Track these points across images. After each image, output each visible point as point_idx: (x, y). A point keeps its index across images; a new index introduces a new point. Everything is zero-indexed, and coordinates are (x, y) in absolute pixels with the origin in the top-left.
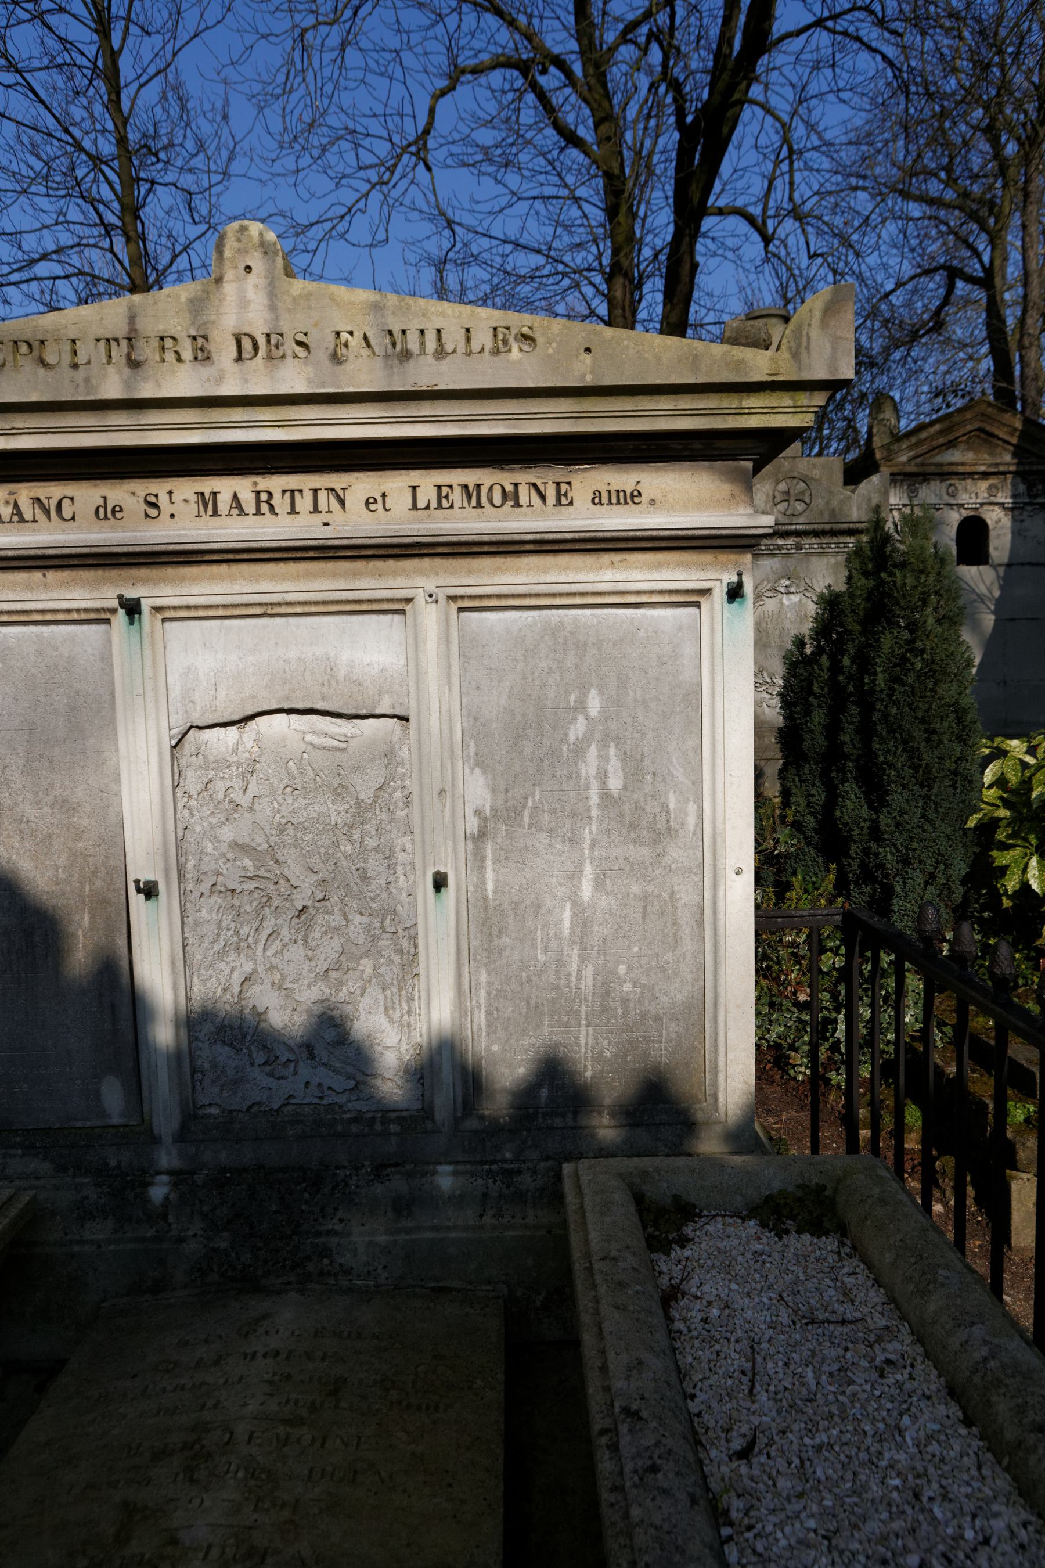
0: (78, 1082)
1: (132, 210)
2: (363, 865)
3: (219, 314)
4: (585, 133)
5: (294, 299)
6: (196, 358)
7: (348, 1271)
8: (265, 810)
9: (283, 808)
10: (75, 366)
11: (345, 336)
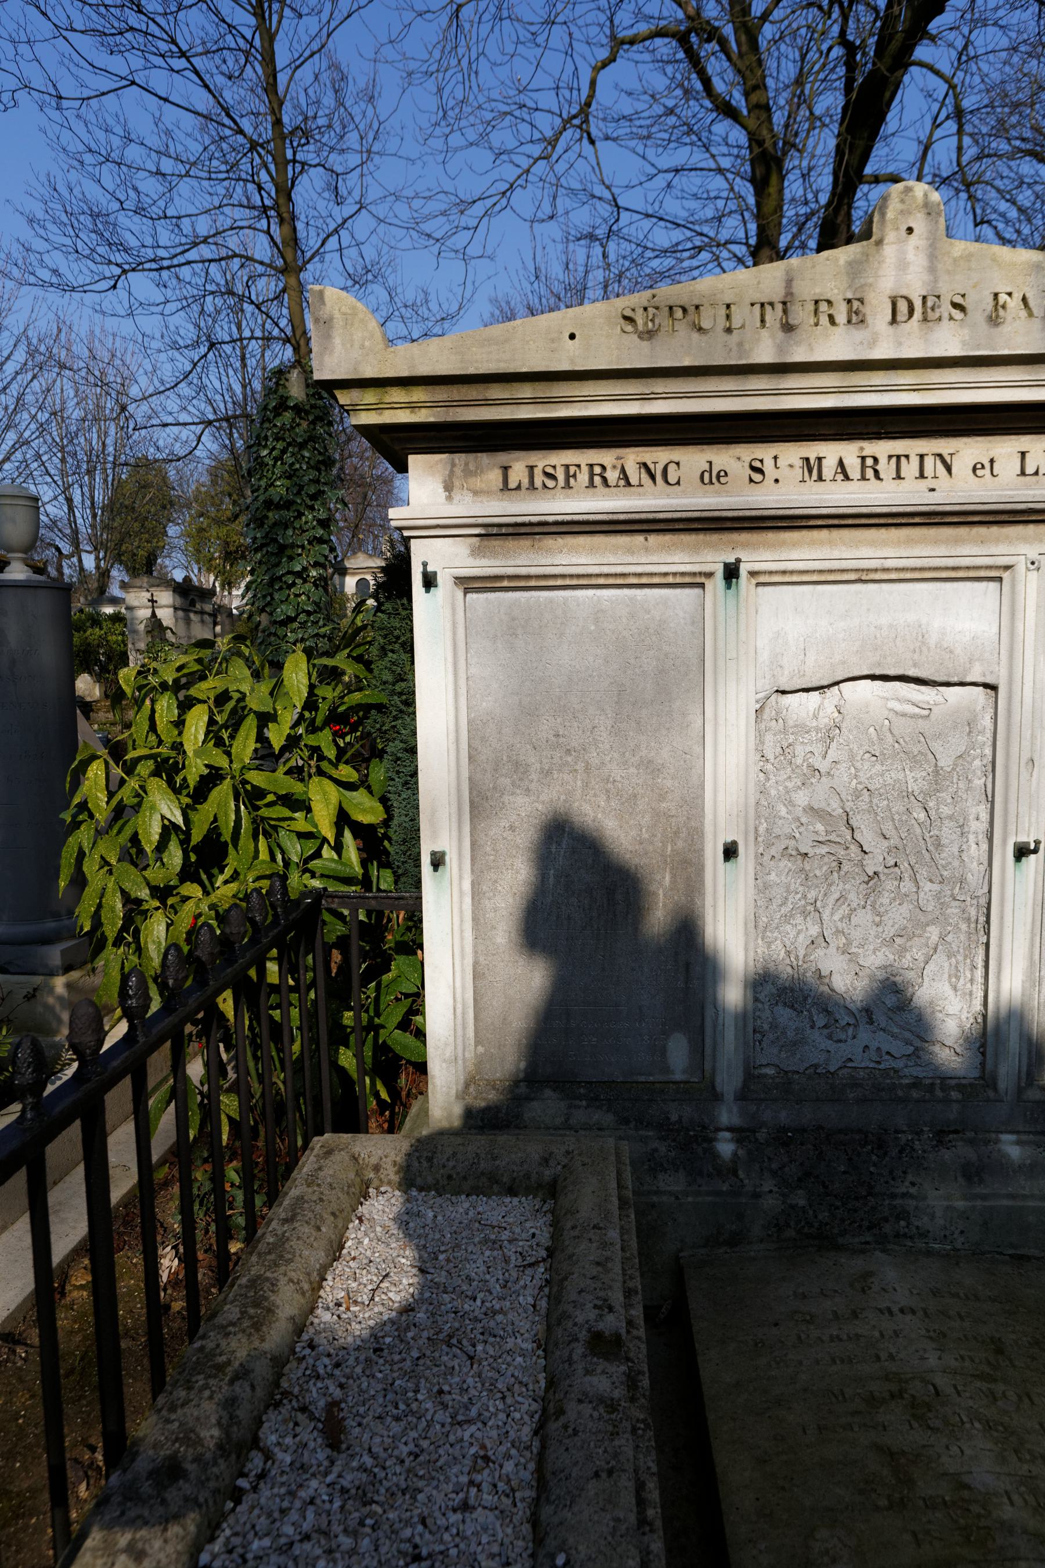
0: (646, 1037)
1: (285, 192)
2: (937, 833)
3: (877, 277)
4: (738, 99)
5: (955, 260)
6: (849, 322)
7: (924, 1235)
8: (843, 777)
9: (861, 774)
10: (729, 330)
11: (1003, 298)
